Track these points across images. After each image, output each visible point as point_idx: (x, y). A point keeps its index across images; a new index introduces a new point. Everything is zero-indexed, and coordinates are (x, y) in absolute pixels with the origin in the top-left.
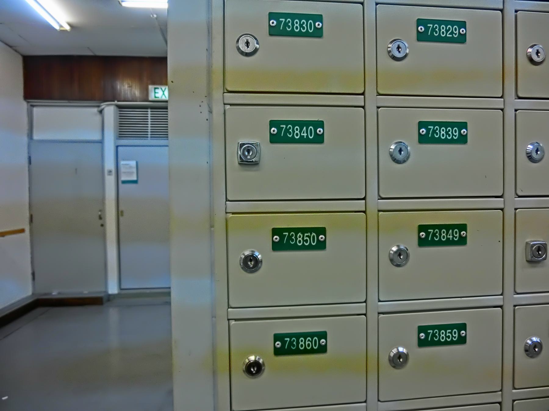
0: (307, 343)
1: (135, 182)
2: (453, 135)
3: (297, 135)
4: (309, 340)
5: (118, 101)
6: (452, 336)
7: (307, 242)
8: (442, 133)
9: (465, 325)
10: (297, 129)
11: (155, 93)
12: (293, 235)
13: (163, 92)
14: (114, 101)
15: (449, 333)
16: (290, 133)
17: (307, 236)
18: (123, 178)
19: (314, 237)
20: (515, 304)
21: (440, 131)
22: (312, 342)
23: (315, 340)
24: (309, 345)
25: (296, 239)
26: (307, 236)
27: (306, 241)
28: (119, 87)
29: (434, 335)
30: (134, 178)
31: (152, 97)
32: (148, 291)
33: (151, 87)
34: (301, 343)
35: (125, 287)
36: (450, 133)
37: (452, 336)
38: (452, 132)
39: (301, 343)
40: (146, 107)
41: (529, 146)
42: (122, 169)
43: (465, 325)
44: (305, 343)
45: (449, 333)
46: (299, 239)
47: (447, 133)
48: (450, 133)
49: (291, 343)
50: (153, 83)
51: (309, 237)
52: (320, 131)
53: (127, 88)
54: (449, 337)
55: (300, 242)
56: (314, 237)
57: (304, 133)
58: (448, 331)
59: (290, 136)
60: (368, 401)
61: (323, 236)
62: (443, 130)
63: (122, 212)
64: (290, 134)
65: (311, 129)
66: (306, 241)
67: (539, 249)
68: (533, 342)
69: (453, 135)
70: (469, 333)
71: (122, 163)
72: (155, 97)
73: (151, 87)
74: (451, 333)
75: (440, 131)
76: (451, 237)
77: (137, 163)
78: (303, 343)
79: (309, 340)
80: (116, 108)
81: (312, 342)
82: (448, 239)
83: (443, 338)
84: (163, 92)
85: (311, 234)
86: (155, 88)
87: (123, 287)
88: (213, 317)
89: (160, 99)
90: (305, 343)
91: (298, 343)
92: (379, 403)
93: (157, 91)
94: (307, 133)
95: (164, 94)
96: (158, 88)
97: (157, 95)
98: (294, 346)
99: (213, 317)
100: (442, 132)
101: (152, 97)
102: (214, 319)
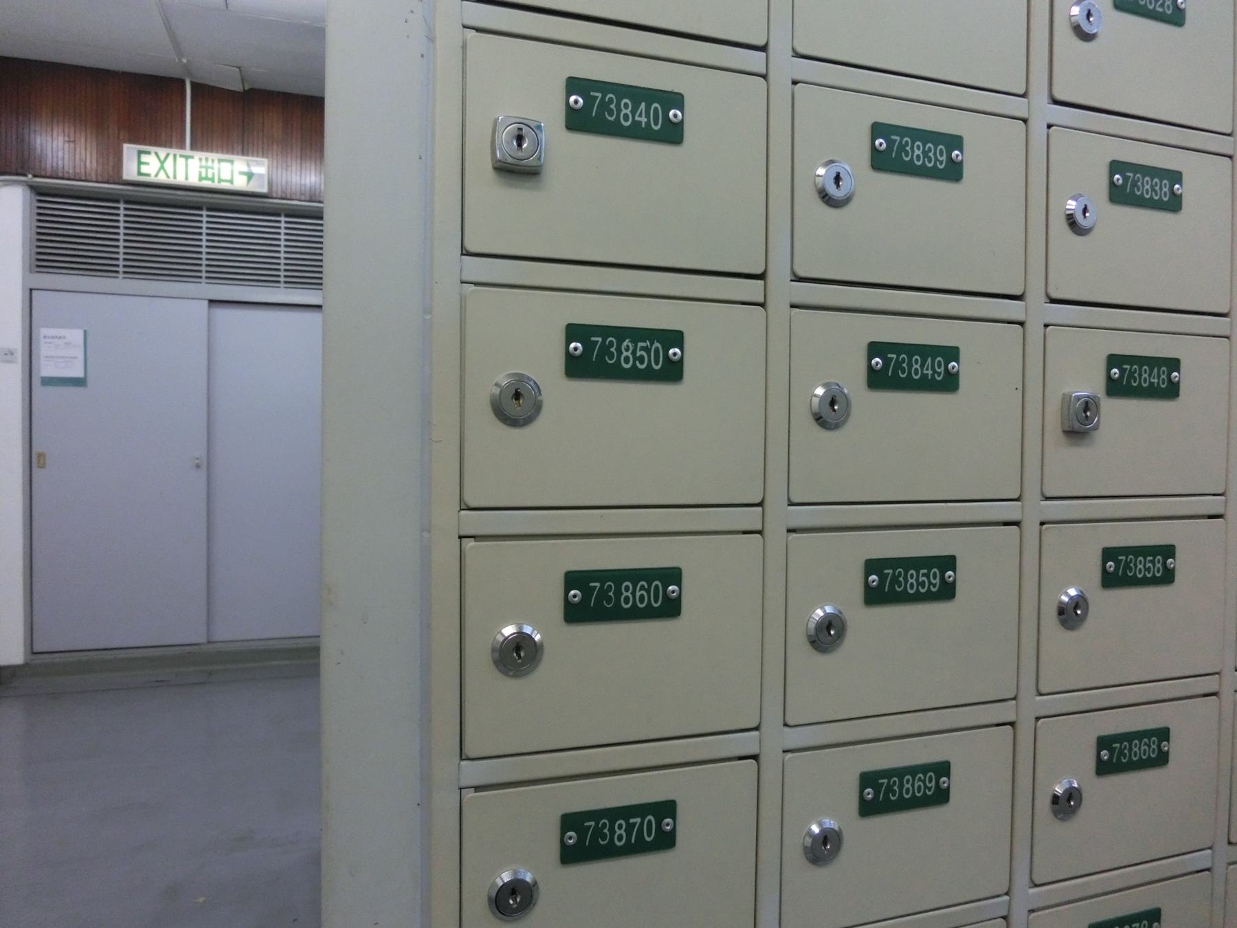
0: (638, 594)
1: (79, 382)
2: (936, 159)
3: (626, 117)
4: (642, 588)
5: (35, 176)
6: (930, 583)
7: (642, 362)
8: (917, 151)
9: (952, 559)
10: (626, 105)
11: (140, 163)
12: (611, 343)
13: (162, 163)
14: (25, 175)
15: (923, 575)
16: (611, 113)
17: (642, 349)
18: (47, 369)
19: (657, 350)
20: (1044, 518)
21: (912, 148)
22: (648, 592)
23: (657, 586)
24: (642, 598)
25: (620, 352)
26: (642, 349)
27: (641, 359)
28: (38, 141)
29: (895, 580)
30: (78, 373)
31: (130, 171)
32: (108, 656)
33: (129, 150)
34: (625, 594)
35: (40, 650)
36: (931, 154)
37: (930, 583)
38: (935, 154)
39: (625, 594)
40: (114, 198)
41: (1070, 202)
42: (44, 350)
43: (952, 559)
44: (634, 594)
45: (923, 575)
46: (625, 354)
47: (925, 153)
48: (931, 154)
49: (603, 594)
50: (131, 141)
51: (647, 350)
52: (675, 116)
53: (60, 148)
54: (923, 584)
55: (627, 360)
56: (657, 350)
57: (640, 115)
58: (922, 571)
59: (612, 119)
60: (763, 728)
61: (677, 350)
62: (918, 148)
63: (41, 455)
64: (611, 115)
65: (656, 109)
66: (641, 359)
67: (1086, 409)
68: (1071, 598)
69: (936, 159)
70: (963, 577)
71: (43, 332)
72: (140, 173)
73: (129, 150)
74: (927, 575)
75: (912, 148)
76: (930, 372)
77: (85, 332)
78: (630, 594)
79: (642, 588)
80: (28, 191)
81: (648, 592)
82: (924, 376)
83: (912, 585)
84: (162, 163)
85: (652, 344)
86: (140, 153)
87: (37, 648)
88: (423, 531)
89: (152, 179)
90: (634, 594)
91: (618, 593)
92: (786, 729)
93: (144, 158)
94: (648, 116)
95: (162, 167)
96: (149, 153)
97: (144, 169)
98: (609, 600)
99: (423, 531)
100: (917, 152)
101: (130, 171)
102: (425, 535)
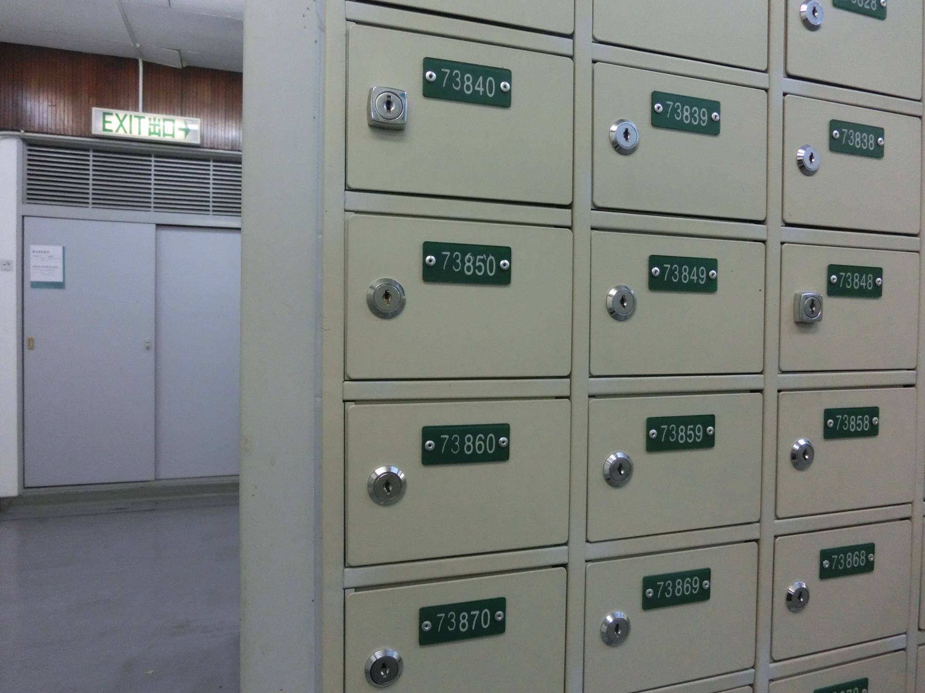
0: (477, 444)
1: (59, 285)
2: (700, 119)
3: (468, 88)
4: (480, 439)
5: (26, 131)
6: (696, 435)
7: (480, 271)
8: (685, 113)
9: (712, 418)
10: (468, 79)
11: (105, 122)
12: (457, 256)
13: (121, 121)
14: (19, 131)
15: (691, 429)
16: (457, 84)
17: (480, 260)
18: (35, 275)
19: (491, 262)
20: (780, 387)
21: (682, 111)
22: (485, 442)
23: (491, 438)
24: (480, 447)
25: (463, 263)
26: (480, 260)
27: (480, 268)
28: (29, 106)
29: (669, 433)
30: (58, 278)
31: (97, 128)
32: (81, 490)
33: (97, 112)
34: (468, 443)
35: (30, 485)
36: (696, 115)
37: (696, 435)
38: (699, 115)
39: (468, 443)
40: (85, 148)
41: (800, 151)
42: (33, 261)
43: (712, 418)
44: (474, 443)
45: (691, 429)
46: (467, 264)
47: (692, 115)
48: (696, 115)
49: (451, 443)
50: (98, 105)
51: (484, 261)
52: (505, 86)
53: (45, 110)
54: (690, 436)
55: (469, 269)
56: (491, 262)
57: (479, 86)
58: (690, 427)
59: (458, 89)
60: (571, 544)
61: (506, 262)
62: (687, 110)
63: (30, 340)
64: (457, 86)
65: (490, 81)
66: (480, 268)
67: (812, 305)
68: (801, 447)
69: (700, 119)
70: (720, 431)
71: (32, 248)
72: (104, 130)
73: (97, 112)
74: (693, 429)
75: (682, 111)
76: (695, 278)
77: (64, 248)
78: (471, 444)
79: (480, 439)
80: (21, 143)
81: (485, 442)
82: (691, 281)
83: (682, 437)
84: (121, 121)
85: (487, 257)
86: (105, 114)
87: (28, 484)
88: (316, 396)
89: (114, 134)
90: (474, 443)
91: (462, 443)
92: (588, 544)
93: (108, 118)
94: (484, 86)
95: (121, 125)
96: (111, 114)
97: (108, 126)
98: (455, 448)
99: (316, 396)
100: (686, 114)
101: (97, 128)
102: (318, 399)
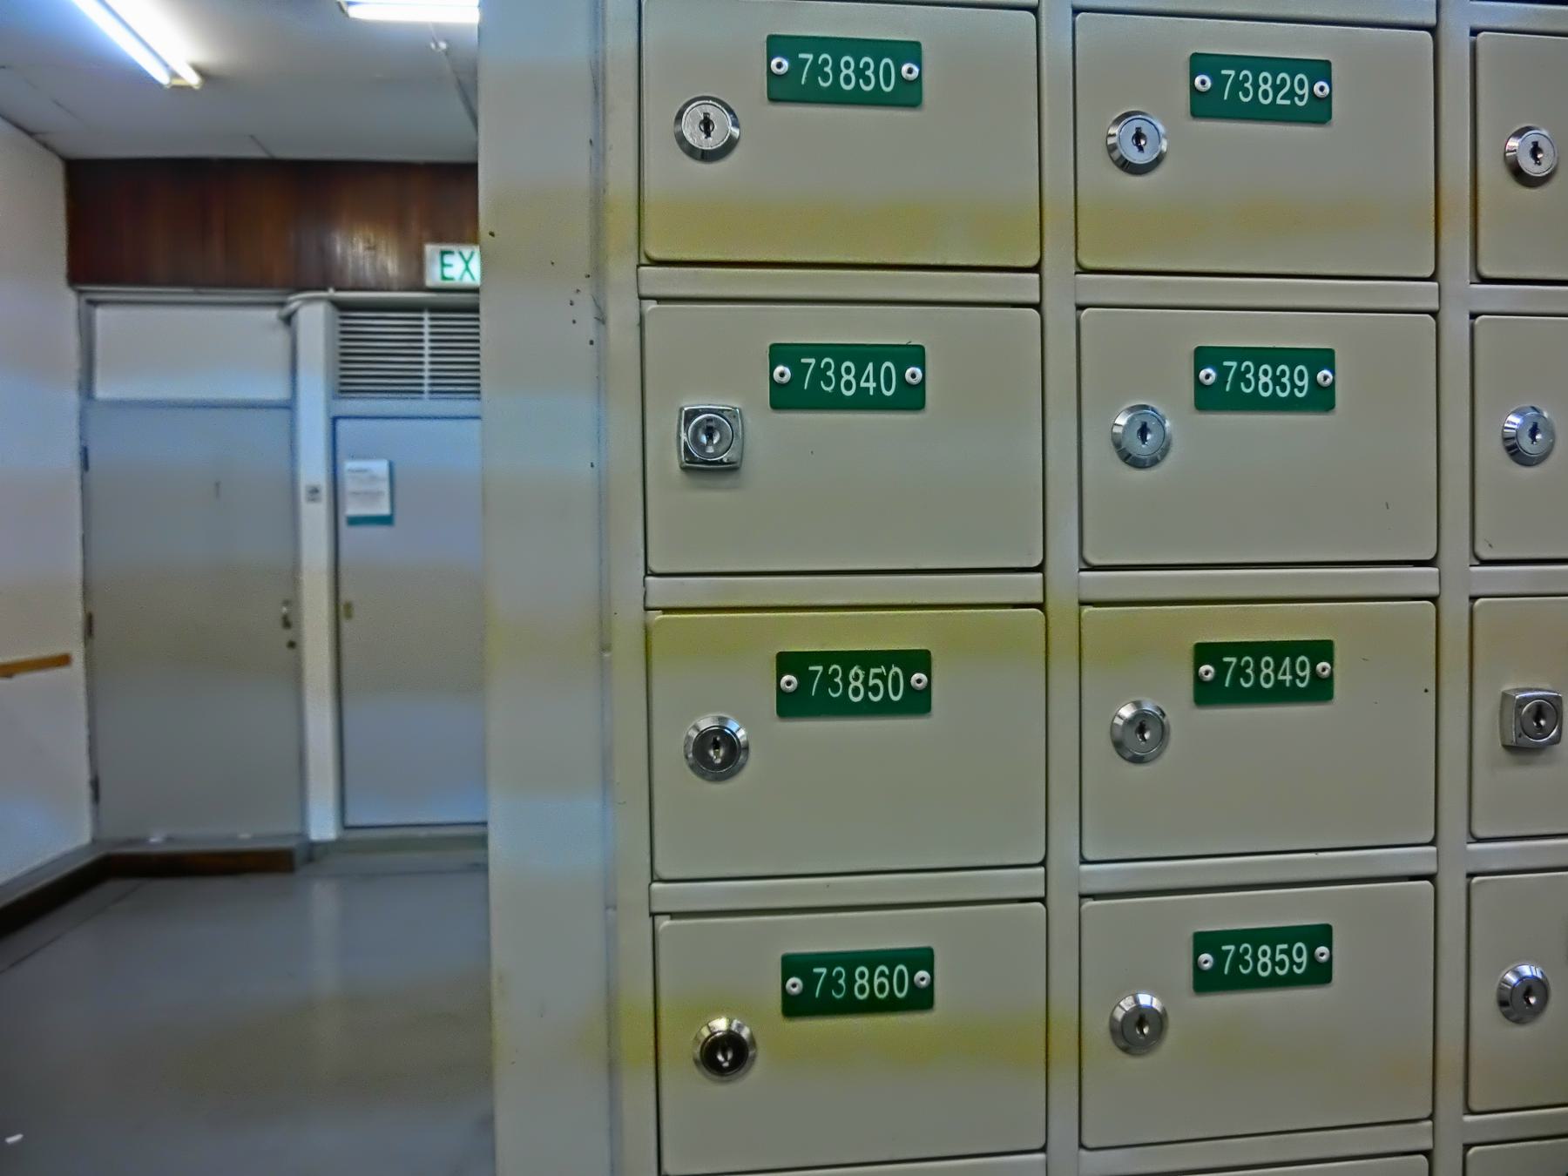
0: (876, 982)
1: (386, 521)
2: (1294, 385)
3: (848, 385)
4: (882, 974)
5: (337, 289)
6: (1292, 962)
7: (876, 694)
8: (1263, 380)
9: (1327, 930)
10: (848, 370)
11: (443, 265)
12: (835, 673)
13: (467, 262)
14: (325, 289)
15: (1282, 952)
16: (828, 382)
17: (876, 676)
18: (352, 509)
19: (896, 677)
20: (1472, 869)
21: (1256, 375)
22: (890, 979)
23: (901, 972)
24: (882, 987)
25: (846, 683)
26: (876, 676)
27: (875, 690)
28: (338, 249)
29: (1239, 959)
30: (384, 509)
31: (433, 277)
32: (423, 833)
33: (431, 250)
34: (859, 982)
35: (358, 822)
36: (1285, 380)
37: (1292, 962)
38: (1291, 379)
39: (859, 982)
40: (416, 307)
41: (1511, 418)
42: (349, 485)
43: (1327, 930)
44: (871, 981)
45: (1282, 952)
46: (853, 684)
47: (1277, 380)
48: (1285, 380)
49: (831, 982)
50: (438, 239)
51: (883, 678)
52: (913, 376)
53: (363, 251)
54: (1281, 964)
55: (856, 691)
56: (896, 677)
57: (867, 380)
58: (1280, 947)
59: (829, 389)
60: (1050, 1148)
61: (923, 677)
62: (1266, 373)
63: (348, 606)
64: (828, 385)
65: (888, 369)
66: (875, 690)
67: (1539, 713)
68: (1522, 979)
69: (1294, 385)
70: (1341, 954)
71: (348, 465)
72: (444, 278)
73: (431, 250)
74: (1288, 952)
75: (1256, 375)
76: (1288, 677)
77: (391, 466)
78: (864, 982)
79: (882, 974)
80: (330, 308)
81: (890, 979)
82: (1280, 684)
83: (1265, 967)
84: (467, 262)
85: (888, 671)
86: (443, 253)
87: (350, 821)
88: (607, 908)
89: (456, 283)
90: (871, 981)
91: (851, 981)
92: (1083, 1153)
93: (447, 259)
94: (877, 379)
95: (467, 269)
96: (451, 253)
97: (448, 272)
98: (839, 989)
99: (607, 908)
100: (1263, 379)
101: (433, 277)
102: (610, 912)
